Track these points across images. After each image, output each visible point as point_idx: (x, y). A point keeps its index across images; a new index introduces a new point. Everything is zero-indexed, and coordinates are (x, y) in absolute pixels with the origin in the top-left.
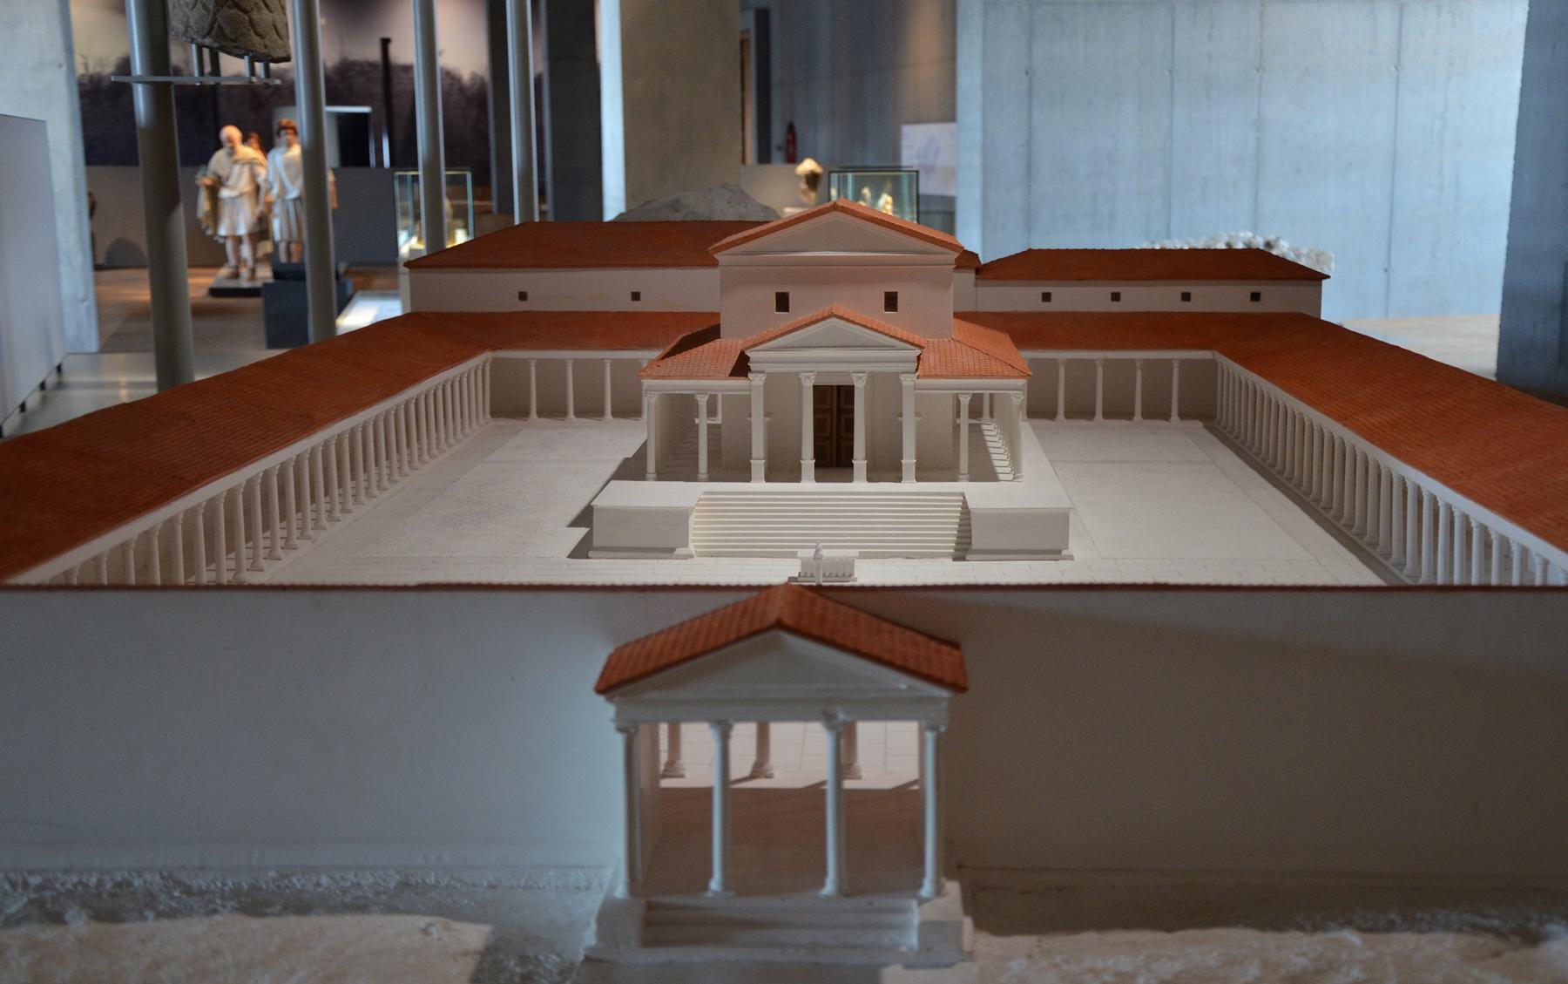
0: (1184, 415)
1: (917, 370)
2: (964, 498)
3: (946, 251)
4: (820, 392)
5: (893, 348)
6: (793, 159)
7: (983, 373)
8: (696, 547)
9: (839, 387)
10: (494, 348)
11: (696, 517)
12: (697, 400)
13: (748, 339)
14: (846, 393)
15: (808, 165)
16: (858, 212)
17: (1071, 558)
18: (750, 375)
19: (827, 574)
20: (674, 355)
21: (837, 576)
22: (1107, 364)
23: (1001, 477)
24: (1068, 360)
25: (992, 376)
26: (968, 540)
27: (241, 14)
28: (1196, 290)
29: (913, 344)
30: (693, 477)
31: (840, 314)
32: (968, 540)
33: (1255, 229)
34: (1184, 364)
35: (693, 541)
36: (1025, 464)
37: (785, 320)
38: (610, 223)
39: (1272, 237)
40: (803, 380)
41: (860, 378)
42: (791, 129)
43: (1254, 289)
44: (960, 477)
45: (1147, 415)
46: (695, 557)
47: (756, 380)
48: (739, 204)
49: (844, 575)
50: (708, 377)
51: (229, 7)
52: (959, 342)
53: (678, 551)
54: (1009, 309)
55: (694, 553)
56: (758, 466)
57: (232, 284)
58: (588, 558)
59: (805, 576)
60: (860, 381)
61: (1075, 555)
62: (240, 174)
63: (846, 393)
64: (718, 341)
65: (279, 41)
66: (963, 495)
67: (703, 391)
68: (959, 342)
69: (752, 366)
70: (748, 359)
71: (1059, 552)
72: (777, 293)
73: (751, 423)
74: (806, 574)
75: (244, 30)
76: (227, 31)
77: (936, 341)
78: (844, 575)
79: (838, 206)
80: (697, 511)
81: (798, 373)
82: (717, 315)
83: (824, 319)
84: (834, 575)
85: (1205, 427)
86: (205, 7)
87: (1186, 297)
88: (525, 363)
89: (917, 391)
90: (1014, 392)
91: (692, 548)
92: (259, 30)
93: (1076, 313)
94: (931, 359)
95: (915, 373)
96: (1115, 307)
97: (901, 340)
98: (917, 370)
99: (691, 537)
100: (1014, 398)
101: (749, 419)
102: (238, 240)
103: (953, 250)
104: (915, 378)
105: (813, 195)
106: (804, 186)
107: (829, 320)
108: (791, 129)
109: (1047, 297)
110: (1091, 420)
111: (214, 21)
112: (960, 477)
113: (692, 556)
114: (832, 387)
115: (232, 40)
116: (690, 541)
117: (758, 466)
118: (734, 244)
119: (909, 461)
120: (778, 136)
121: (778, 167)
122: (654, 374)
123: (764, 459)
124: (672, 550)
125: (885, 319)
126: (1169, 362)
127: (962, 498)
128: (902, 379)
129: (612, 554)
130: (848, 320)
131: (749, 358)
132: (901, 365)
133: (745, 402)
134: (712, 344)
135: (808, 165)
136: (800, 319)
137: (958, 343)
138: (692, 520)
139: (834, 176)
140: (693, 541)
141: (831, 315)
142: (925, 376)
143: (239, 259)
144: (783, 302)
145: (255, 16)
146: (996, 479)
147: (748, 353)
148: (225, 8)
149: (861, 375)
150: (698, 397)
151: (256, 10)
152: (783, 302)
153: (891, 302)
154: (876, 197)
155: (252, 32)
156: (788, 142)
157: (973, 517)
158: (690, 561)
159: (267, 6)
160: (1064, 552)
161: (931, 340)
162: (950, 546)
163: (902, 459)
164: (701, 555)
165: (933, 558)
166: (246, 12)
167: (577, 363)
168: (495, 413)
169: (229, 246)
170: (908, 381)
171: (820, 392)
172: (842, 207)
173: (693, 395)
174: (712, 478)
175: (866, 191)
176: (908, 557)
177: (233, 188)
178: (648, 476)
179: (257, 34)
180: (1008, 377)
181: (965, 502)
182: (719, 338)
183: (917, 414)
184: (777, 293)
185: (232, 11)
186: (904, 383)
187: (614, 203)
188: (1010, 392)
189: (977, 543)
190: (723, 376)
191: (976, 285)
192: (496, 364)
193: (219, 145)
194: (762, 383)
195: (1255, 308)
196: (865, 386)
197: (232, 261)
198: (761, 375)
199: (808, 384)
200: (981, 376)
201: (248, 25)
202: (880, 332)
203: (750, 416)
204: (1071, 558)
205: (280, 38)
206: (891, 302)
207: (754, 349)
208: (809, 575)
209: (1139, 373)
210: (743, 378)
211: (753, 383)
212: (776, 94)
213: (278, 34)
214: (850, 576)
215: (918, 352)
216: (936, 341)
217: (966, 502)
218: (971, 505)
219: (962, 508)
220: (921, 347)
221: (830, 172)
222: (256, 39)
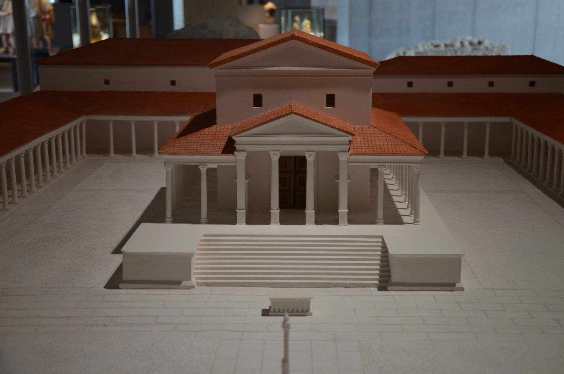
0: (491, 154)
1: (349, 150)
2: (383, 239)
4: (284, 160)
7: (395, 152)
8: (197, 278)
9: (295, 157)
10: (87, 114)
11: (197, 259)
12: (200, 169)
13: (235, 125)
14: (300, 161)
15: (270, 5)
16: (309, 40)
17: (462, 289)
18: (236, 153)
19: (290, 310)
20: (185, 135)
21: (297, 311)
22: (448, 124)
23: (405, 219)
24: (425, 123)
25: (401, 154)
26: (388, 274)
29: (347, 132)
30: (196, 221)
31: (297, 112)
32: (388, 274)
33: (473, 34)
34: (493, 125)
35: (195, 274)
36: (423, 216)
37: (260, 113)
38: (177, 31)
39: (481, 39)
40: (272, 156)
41: (311, 155)
43: (532, 79)
44: (378, 221)
45: (471, 153)
46: (197, 287)
47: (240, 156)
49: (302, 311)
50: (207, 154)
52: (375, 128)
53: (184, 283)
54: (389, 91)
55: (195, 284)
56: (241, 213)
57: (5, 56)
58: (119, 288)
59: (274, 312)
60: (310, 157)
61: (465, 288)
62: (8, 4)
63: (300, 161)
64: (215, 126)
66: (382, 237)
67: (204, 163)
68: (375, 128)
69: (238, 147)
70: (234, 141)
71: (453, 285)
72: (254, 95)
73: (236, 183)
74: (275, 309)
77: (360, 127)
78: (302, 311)
79: (295, 36)
80: (198, 254)
81: (269, 152)
83: (286, 115)
84: (295, 310)
85: (505, 162)
88: (107, 123)
89: (349, 164)
90: (416, 165)
91: (194, 281)
93: (426, 94)
94: (359, 140)
95: (348, 152)
96: (450, 90)
97: (339, 130)
98: (349, 150)
99: (193, 271)
100: (415, 169)
101: (235, 180)
102: (8, 36)
103: (372, 66)
104: (348, 155)
106: (267, 15)
107: (289, 116)
109: (410, 84)
110: (436, 157)
112: (378, 221)
113: (193, 287)
114: (291, 157)
116: (192, 274)
117: (241, 213)
118: (225, 61)
119: (343, 210)
121: (256, 7)
122: (170, 152)
123: (245, 209)
124: (179, 283)
125: (325, 112)
126: (484, 124)
127: (381, 240)
128: (339, 155)
129: (136, 286)
130: (302, 116)
131: (235, 141)
132: (339, 146)
133: (232, 170)
134: (211, 128)
135: (270, 5)
136: (269, 112)
137: (375, 129)
138: (194, 261)
139: (283, 12)
140: (195, 274)
141: (292, 113)
142: (355, 154)
143: (9, 45)
144: (258, 101)
146: (401, 222)
147: (234, 138)
149: (311, 153)
150: (200, 167)
152: (258, 101)
153: (330, 100)
154: (302, 20)
157: (391, 260)
158: (192, 291)
160: (457, 285)
161: (356, 126)
162: (375, 279)
164: (200, 285)
165: (364, 287)
167: (137, 123)
168: (90, 151)
169: (4, 38)
170: (343, 157)
171: (284, 160)
172: (298, 36)
173: (197, 166)
174: (211, 221)
175: (297, 18)
176: (346, 286)
177: (5, 11)
178: (167, 220)
180: (412, 155)
181: (384, 243)
182: (216, 124)
183: (349, 177)
184: (254, 95)
186: (341, 159)
187: (179, 22)
188: (413, 165)
189: (395, 278)
190: (217, 153)
192: (88, 122)
194: (244, 158)
195: (532, 90)
196: (314, 161)
197: (5, 45)
198: (242, 153)
199: (275, 159)
200: (394, 154)
202: (325, 124)
203: (236, 178)
204: (462, 289)
206: (330, 100)
207: (237, 136)
208: (277, 310)
209: (466, 131)
210: (231, 155)
211: (238, 158)
214: (307, 311)
215: (350, 137)
216: (360, 127)
217: (386, 247)
218: (393, 250)
219: (382, 248)
220: (352, 134)
221: (282, 9)
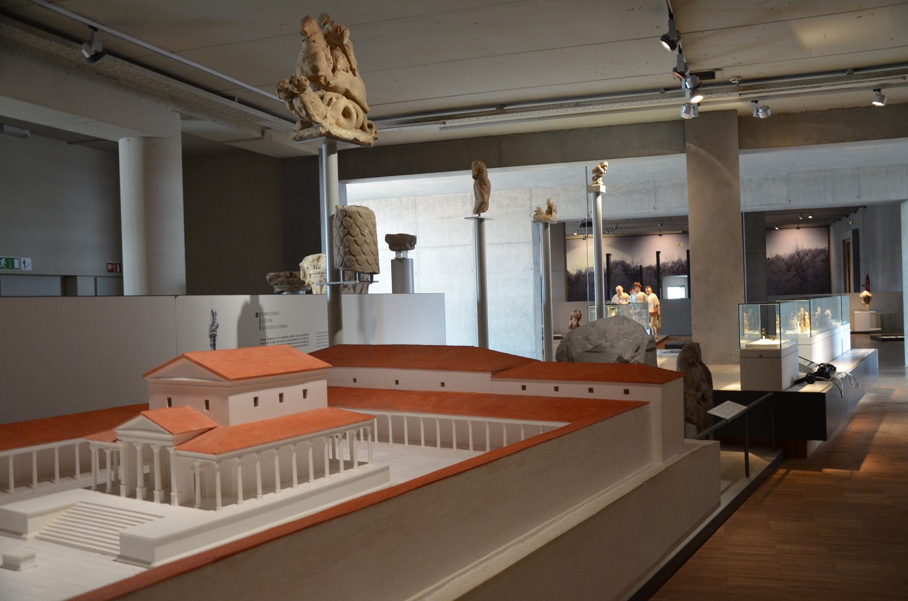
3: (222, 379)
5: (164, 433)
6: (858, 290)
15: (865, 293)
27: (352, 257)
28: (632, 388)
42: (868, 278)
48: (620, 324)
51: (348, 255)
65: (369, 266)
75: (353, 263)
76: (347, 264)
82: (492, 380)
86: (341, 256)
87: (627, 392)
92: (359, 263)
105: (867, 305)
108: (868, 278)
111: (343, 260)
115: (349, 267)
120: (863, 281)
145: (358, 257)
148: (347, 255)
151: (358, 256)
155: (356, 264)
156: (866, 283)
159: (363, 253)
163: (171, 492)
166: (354, 256)
179: (358, 264)
185: (349, 256)
191: (492, 380)
193: (615, 293)
201: (355, 261)
205: (370, 265)
212: (862, 264)
213: (369, 264)
222: (358, 266)
